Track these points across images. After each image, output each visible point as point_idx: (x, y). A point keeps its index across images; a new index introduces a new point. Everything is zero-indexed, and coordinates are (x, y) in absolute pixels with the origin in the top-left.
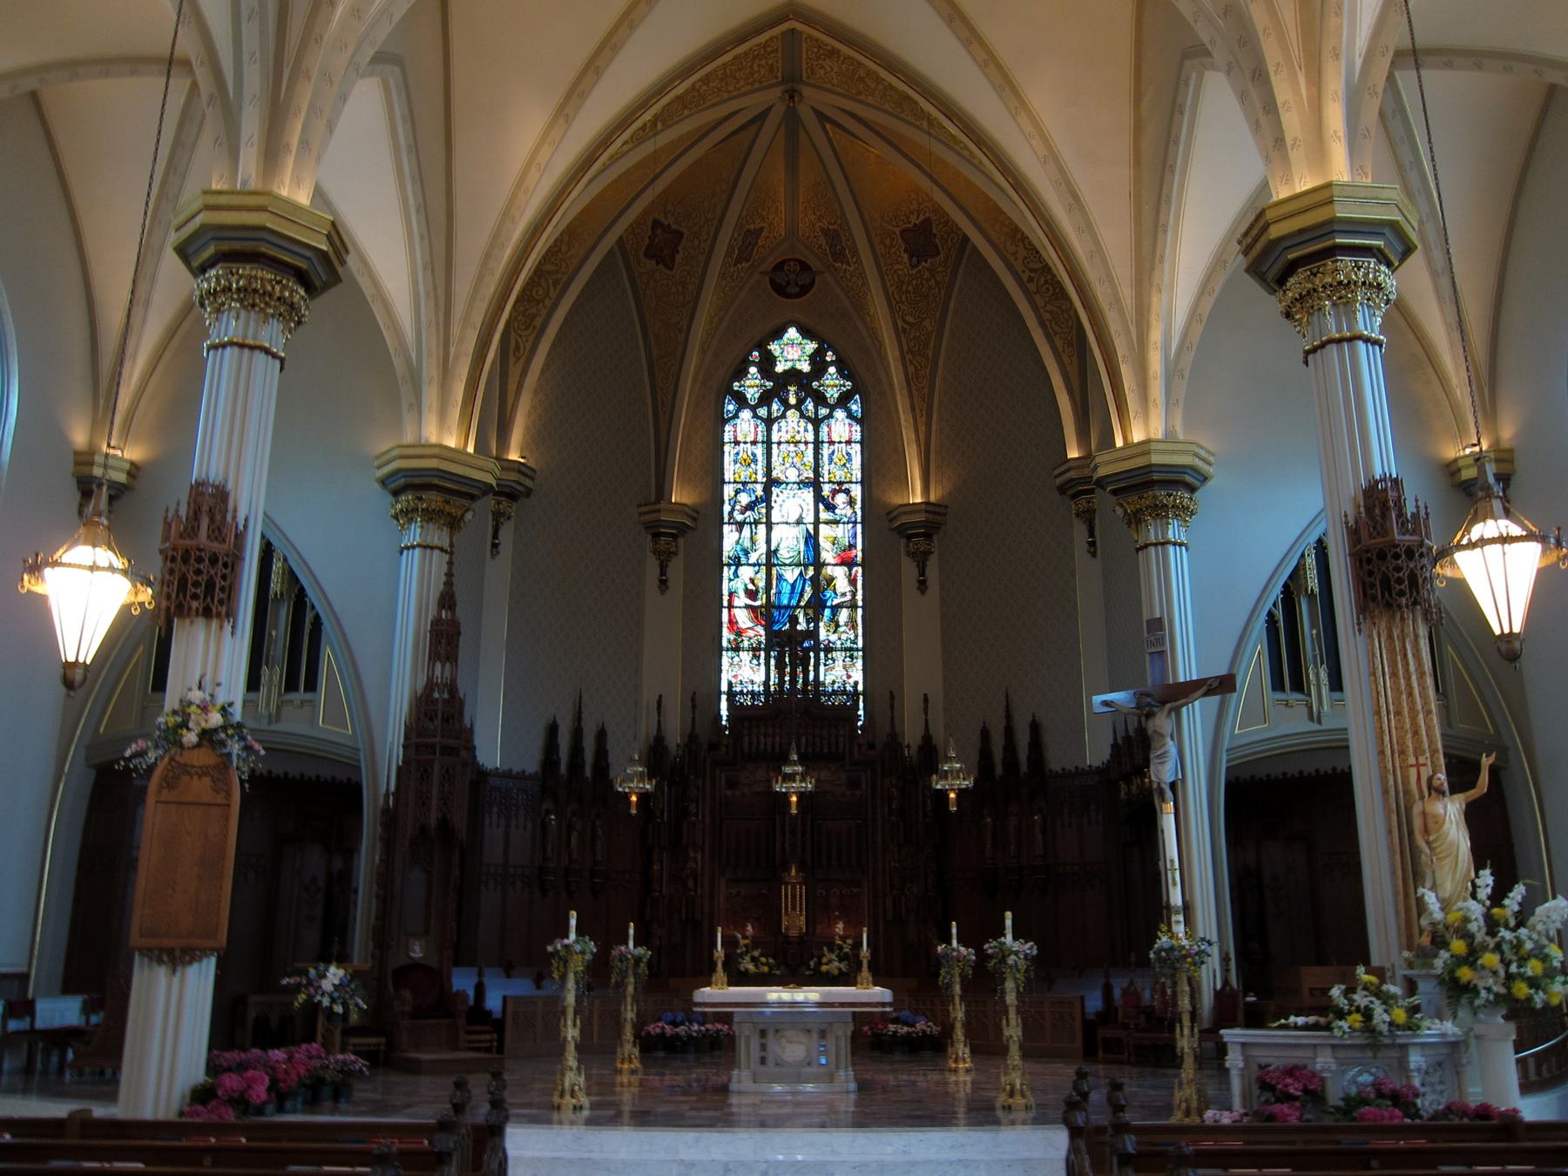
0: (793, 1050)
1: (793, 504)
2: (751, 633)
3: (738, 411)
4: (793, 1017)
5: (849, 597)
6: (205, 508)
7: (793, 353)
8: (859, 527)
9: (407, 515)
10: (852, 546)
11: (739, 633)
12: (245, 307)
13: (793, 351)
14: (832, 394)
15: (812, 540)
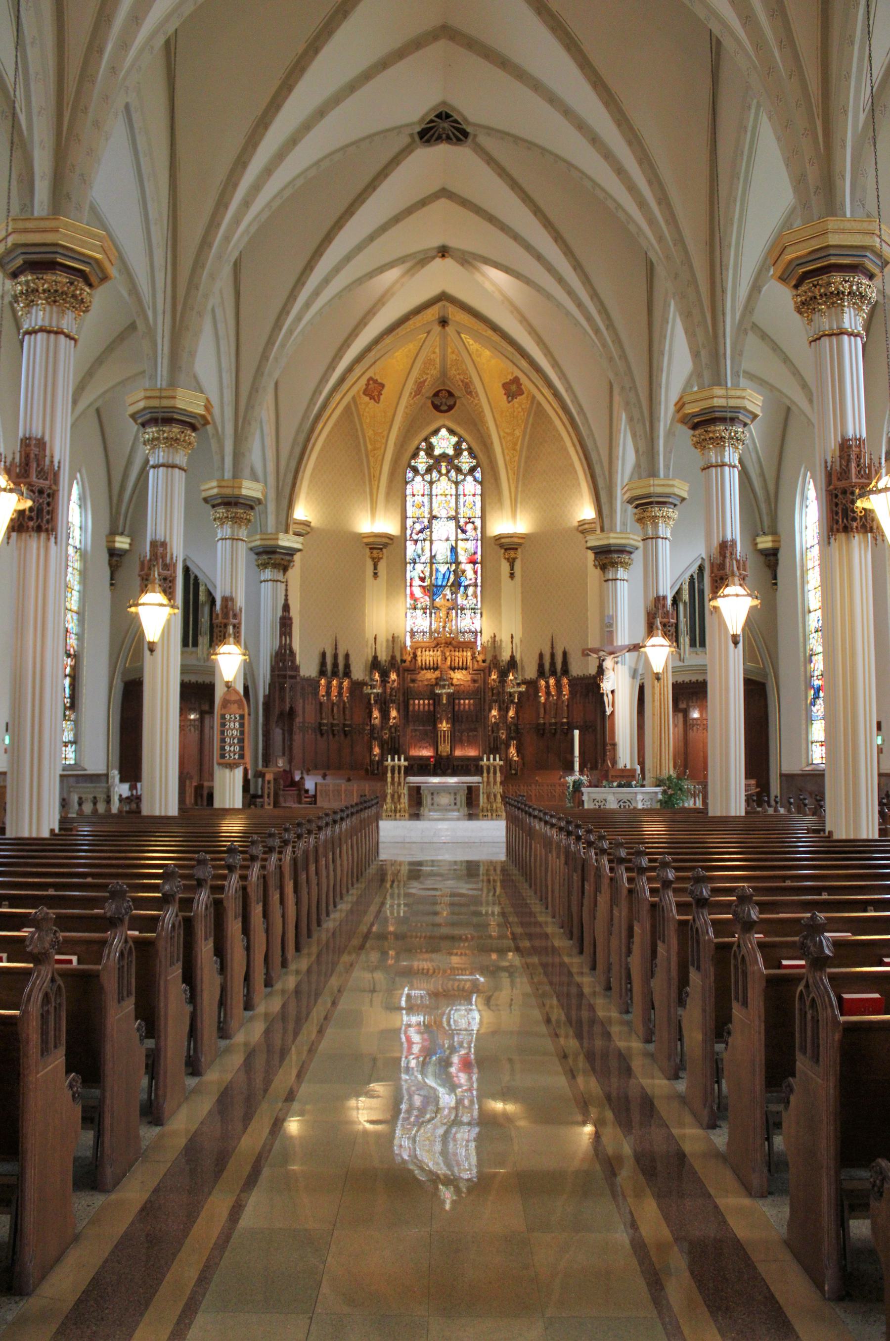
0: (444, 800)
1: (444, 530)
2: (422, 600)
3: (414, 477)
4: (445, 789)
5: (473, 581)
6: (32, 456)
7: (444, 444)
8: (479, 542)
9: (264, 566)
10: (475, 553)
11: (416, 600)
12: (49, 303)
13: (444, 443)
14: (465, 467)
15: (454, 550)
